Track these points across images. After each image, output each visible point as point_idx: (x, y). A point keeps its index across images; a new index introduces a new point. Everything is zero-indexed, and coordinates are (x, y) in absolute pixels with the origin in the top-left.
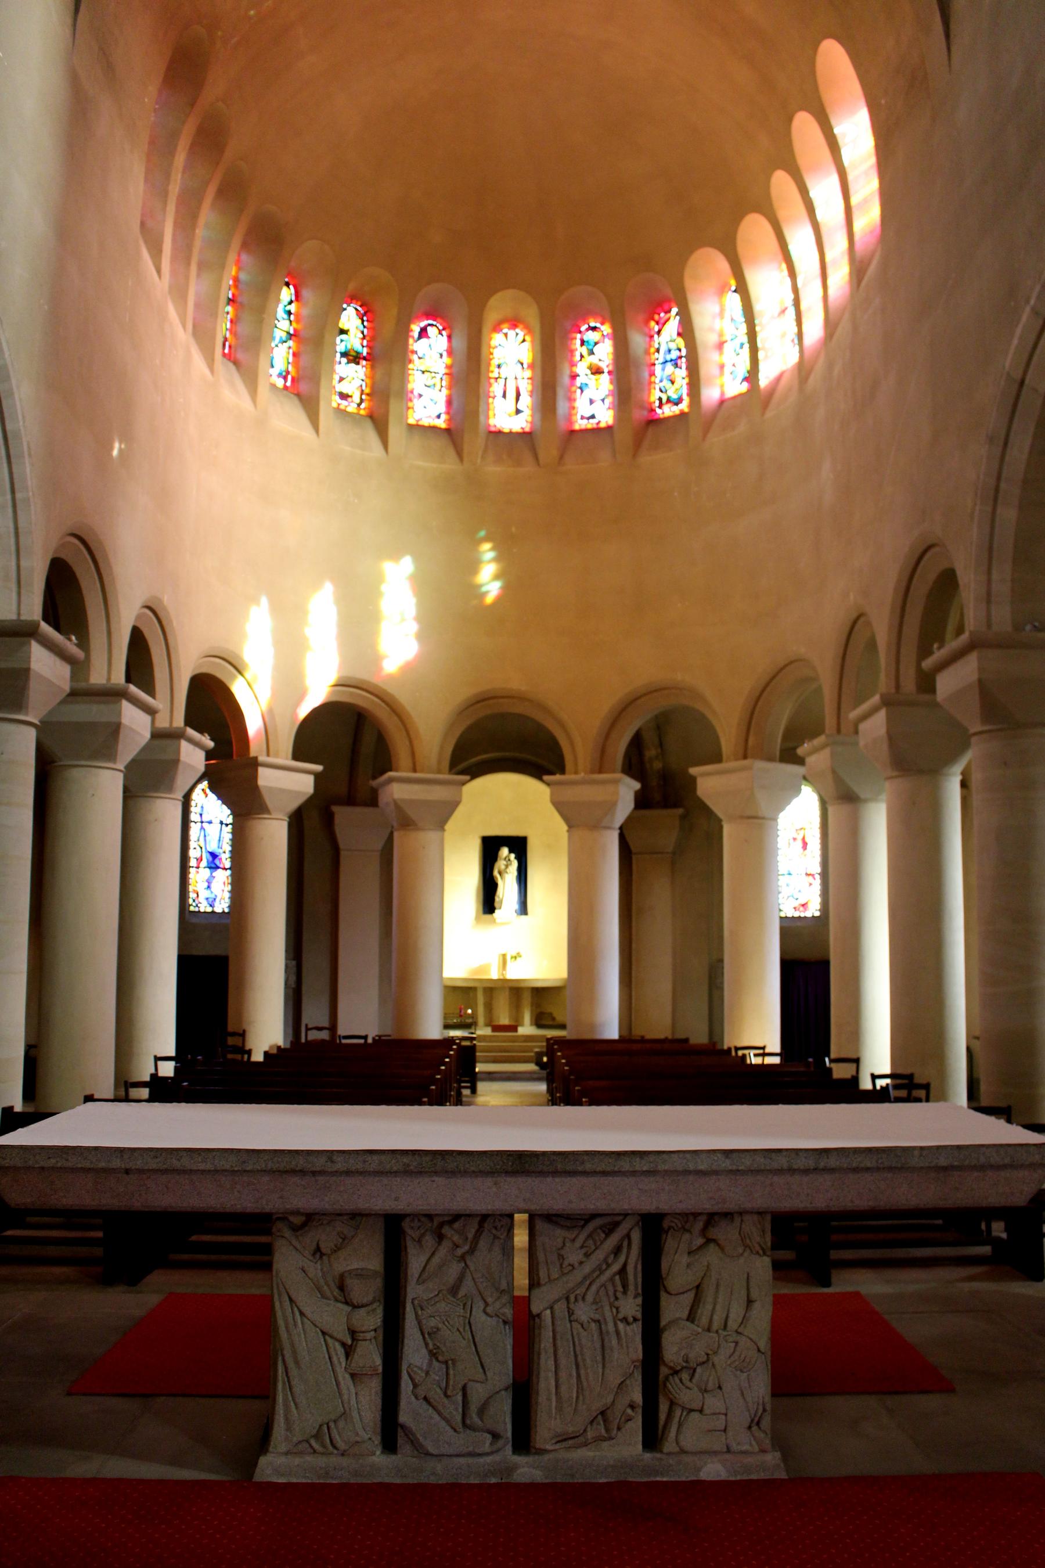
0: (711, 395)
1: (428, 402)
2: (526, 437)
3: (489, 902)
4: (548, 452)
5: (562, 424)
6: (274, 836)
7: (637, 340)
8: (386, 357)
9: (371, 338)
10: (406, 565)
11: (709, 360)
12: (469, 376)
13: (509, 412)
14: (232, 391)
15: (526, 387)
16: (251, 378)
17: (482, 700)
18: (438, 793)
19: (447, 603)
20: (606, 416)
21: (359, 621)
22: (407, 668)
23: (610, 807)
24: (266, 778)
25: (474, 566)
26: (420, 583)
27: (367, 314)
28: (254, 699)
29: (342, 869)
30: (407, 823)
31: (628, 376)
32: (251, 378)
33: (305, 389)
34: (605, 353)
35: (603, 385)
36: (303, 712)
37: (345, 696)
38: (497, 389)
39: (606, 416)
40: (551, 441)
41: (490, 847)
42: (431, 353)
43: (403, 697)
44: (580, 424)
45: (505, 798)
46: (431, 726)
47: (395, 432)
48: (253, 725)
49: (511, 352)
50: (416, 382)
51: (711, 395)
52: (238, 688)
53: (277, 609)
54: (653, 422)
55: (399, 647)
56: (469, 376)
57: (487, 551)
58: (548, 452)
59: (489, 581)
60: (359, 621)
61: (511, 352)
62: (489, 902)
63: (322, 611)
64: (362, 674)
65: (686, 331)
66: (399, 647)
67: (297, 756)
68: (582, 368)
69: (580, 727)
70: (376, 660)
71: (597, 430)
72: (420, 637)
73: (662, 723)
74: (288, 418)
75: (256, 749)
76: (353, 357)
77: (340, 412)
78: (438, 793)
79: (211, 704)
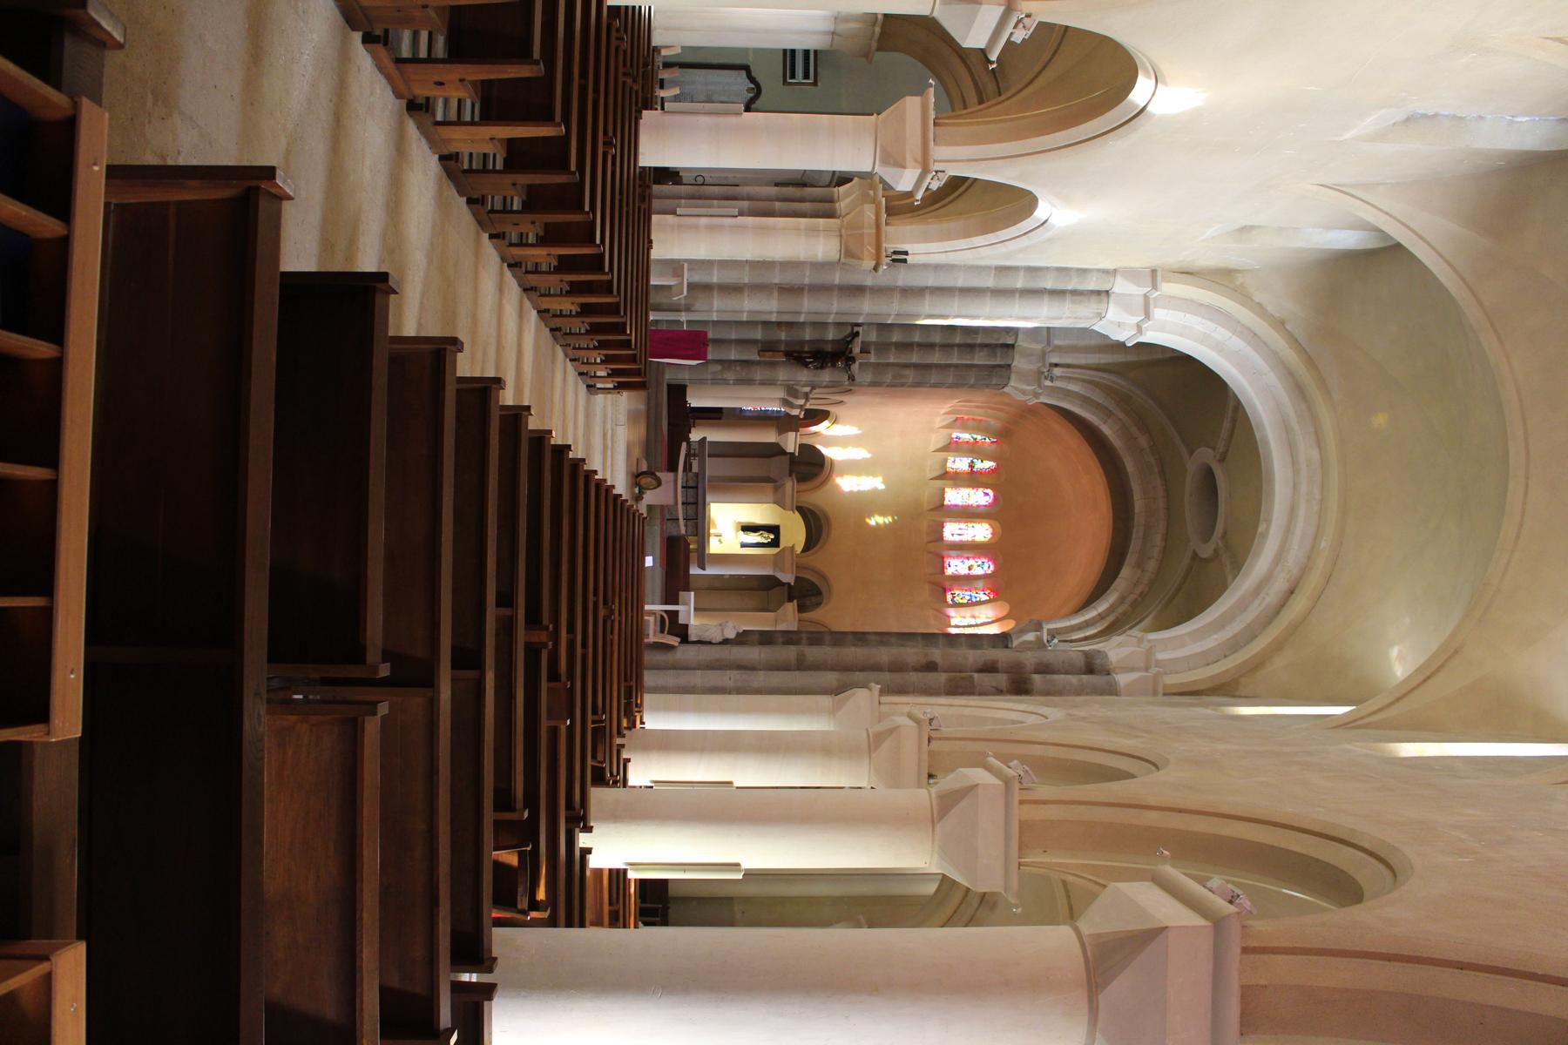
0: (951, 612)
1: (956, 496)
2: (941, 538)
3: (747, 528)
4: (932, 547)
5: (945, 553)
6: (768, 436)
7: (980, 584)
8: (972, 479)
9: (981, 472)
10: (882, 487)
11: (967, 612)
12: (967, 514)
13: (953, 531)
14: (939, 421)
15: (964, 538)
16: (950, 426)
17: (828, 519)
18: (788, 501)
19: (867, 503)
20: (949, 571)
21: (855, 468)
22: (838, 486)
23: (782, 571)
24: (791, 435)
25: (882, 514)
26: (875, 491)
27: (992, 471)
28: (823, 428)
29: (761, 460)
30: (776, 489)
31: (967, 580)
32: (950, 426)
33: (952, 447)
34: (977, 571)
35: (963, 570)
36: (819, 447)
37: (827, 464)
38: (963, 525)
39: (949, 571)
40: (939, 549)
41: (774, 529)
42: (979, 497)
43: (828, 487)
44: (947, 561)
45: (795, 533)
46: (815, 498)
47: (939, 483)
48: (813, 429)
49: (981, 532)
50: (964, 492)
51: (951, 612)
52: (826, 423)
53: (857, 436)
54: (945, 591)
55: (847, 484)
56: (967, 514)
57: (888, 520)
58: (932, 547)
59: (876, 520)
60: (855, 468)
61: (981, 532)
62: (747, 528)
63: (859, 453)
64: (836, 469)
65: (980, 603)
66: (847, 484)
67: (801, 446)
68: (971, 562)
69: (817, 559)
70: (841, 475)
71: (943, 568)
72: (851, 492)
73: (819, 593)
74: (938, 439)
75: (803, 430)
76: (971, 465)
77: (946, 461)
78: (788, 501)
79: (816, 416)
